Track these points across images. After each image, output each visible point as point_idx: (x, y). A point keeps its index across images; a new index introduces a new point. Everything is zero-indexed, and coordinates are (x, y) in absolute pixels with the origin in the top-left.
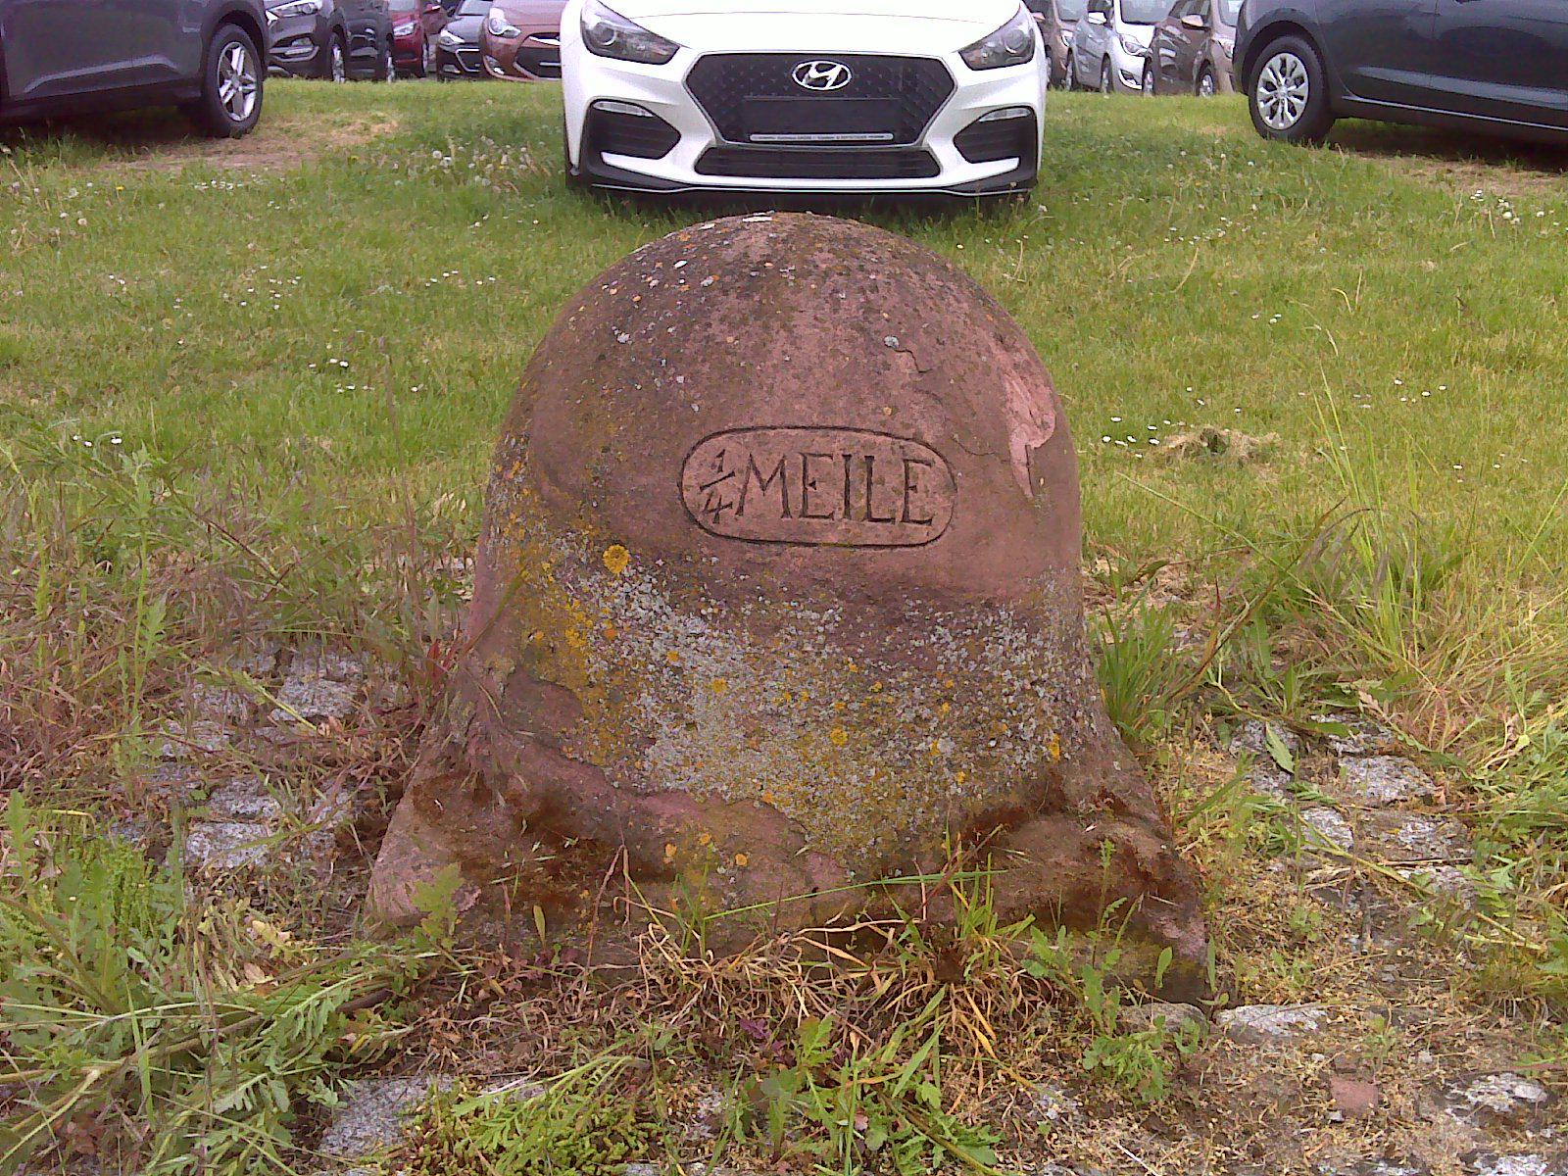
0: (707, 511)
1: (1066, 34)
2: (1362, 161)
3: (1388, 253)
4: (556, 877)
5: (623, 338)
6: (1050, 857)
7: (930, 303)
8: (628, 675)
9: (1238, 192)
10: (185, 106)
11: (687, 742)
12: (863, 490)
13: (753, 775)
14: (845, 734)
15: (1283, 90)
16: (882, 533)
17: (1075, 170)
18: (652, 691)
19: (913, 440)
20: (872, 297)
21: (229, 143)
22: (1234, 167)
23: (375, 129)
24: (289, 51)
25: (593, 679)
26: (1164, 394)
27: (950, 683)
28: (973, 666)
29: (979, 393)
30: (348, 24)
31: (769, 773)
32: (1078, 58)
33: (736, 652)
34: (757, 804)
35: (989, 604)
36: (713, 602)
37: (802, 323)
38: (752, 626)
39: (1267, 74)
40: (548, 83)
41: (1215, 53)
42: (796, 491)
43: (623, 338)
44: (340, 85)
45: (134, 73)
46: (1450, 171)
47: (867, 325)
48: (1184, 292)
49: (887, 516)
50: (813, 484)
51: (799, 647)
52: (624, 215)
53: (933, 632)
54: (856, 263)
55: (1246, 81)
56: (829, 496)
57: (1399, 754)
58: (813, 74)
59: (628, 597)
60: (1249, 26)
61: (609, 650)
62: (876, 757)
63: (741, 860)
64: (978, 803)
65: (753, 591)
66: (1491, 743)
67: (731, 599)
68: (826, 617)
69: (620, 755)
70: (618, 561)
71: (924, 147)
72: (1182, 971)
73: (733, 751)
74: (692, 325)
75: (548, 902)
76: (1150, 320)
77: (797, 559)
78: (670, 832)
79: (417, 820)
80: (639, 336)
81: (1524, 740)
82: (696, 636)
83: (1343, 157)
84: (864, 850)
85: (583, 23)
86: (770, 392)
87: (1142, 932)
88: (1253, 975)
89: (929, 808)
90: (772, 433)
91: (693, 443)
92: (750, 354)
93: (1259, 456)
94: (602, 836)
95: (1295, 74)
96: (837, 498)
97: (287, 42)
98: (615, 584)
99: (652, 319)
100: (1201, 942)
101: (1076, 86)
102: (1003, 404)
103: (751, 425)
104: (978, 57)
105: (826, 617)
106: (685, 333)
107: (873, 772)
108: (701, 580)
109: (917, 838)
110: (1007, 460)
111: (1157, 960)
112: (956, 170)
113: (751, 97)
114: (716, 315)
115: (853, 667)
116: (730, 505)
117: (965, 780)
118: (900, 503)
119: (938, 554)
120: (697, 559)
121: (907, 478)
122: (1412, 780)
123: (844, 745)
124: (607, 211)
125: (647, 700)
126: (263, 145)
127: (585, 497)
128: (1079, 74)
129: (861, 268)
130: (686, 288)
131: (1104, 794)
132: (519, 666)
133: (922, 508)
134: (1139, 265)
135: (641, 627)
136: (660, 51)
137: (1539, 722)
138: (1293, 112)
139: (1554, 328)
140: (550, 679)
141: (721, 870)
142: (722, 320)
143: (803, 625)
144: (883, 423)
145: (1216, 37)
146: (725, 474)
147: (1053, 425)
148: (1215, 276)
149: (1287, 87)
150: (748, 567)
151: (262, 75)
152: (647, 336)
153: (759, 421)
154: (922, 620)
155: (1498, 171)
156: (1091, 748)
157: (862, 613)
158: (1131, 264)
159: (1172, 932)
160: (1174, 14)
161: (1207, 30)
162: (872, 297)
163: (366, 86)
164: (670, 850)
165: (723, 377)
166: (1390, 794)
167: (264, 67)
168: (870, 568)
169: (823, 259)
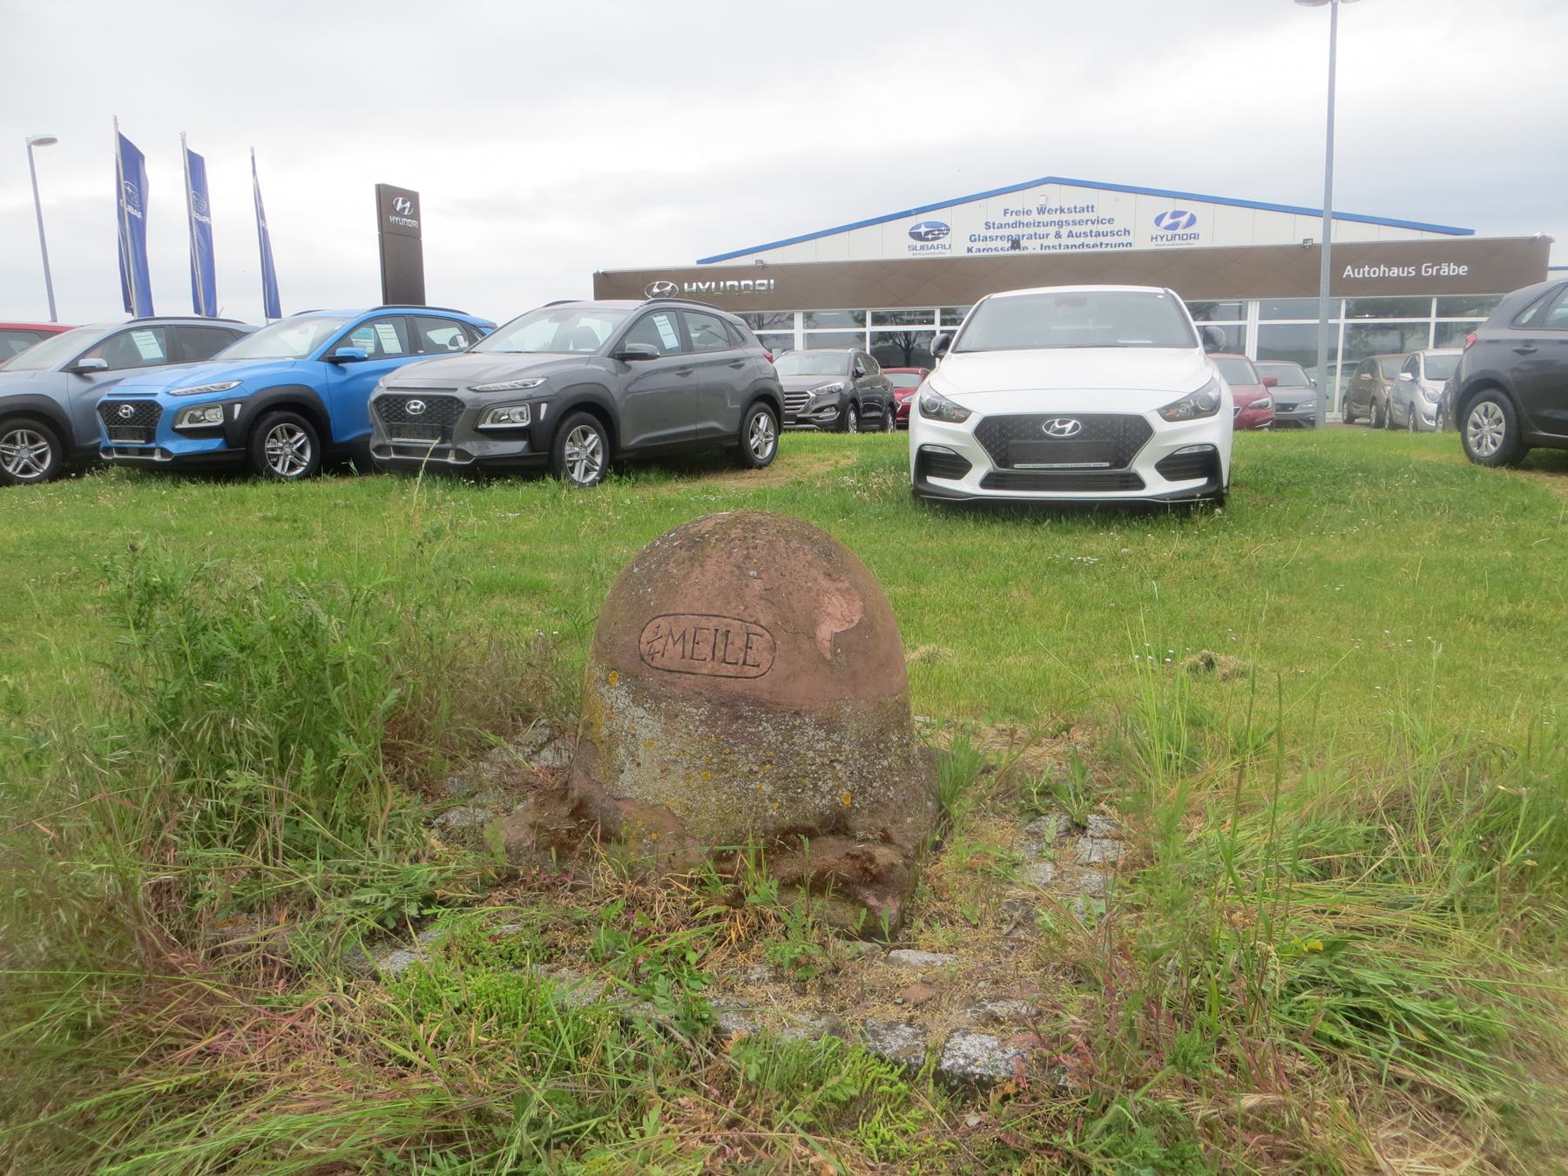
10: (729, 451)
15: (1487, 428)
16: (731, 670)
21: (753, 472)
24: (821, 415)
31: (670, 792)
32: (1394, 405)
35: (797, 713)
37: (710, 565)
39: (1475, 416)
44: (853, 435)
45: (696, 432)
56: (705, 650)
62: (726, 788)
63: (654, 836)
64: (788, 819)
67: (657, 699)
96: (708, 650)
97: (820, 410)
104: (1171, 413)
106: (658, 566)
112: (1157, 486)
119: (763, 684)
125: (622, 750)
138: (1494, 443)
143: (689, 715)
150: (664, 683)
151: (779, 429)
154: (753, 718)
168: (724, 687)
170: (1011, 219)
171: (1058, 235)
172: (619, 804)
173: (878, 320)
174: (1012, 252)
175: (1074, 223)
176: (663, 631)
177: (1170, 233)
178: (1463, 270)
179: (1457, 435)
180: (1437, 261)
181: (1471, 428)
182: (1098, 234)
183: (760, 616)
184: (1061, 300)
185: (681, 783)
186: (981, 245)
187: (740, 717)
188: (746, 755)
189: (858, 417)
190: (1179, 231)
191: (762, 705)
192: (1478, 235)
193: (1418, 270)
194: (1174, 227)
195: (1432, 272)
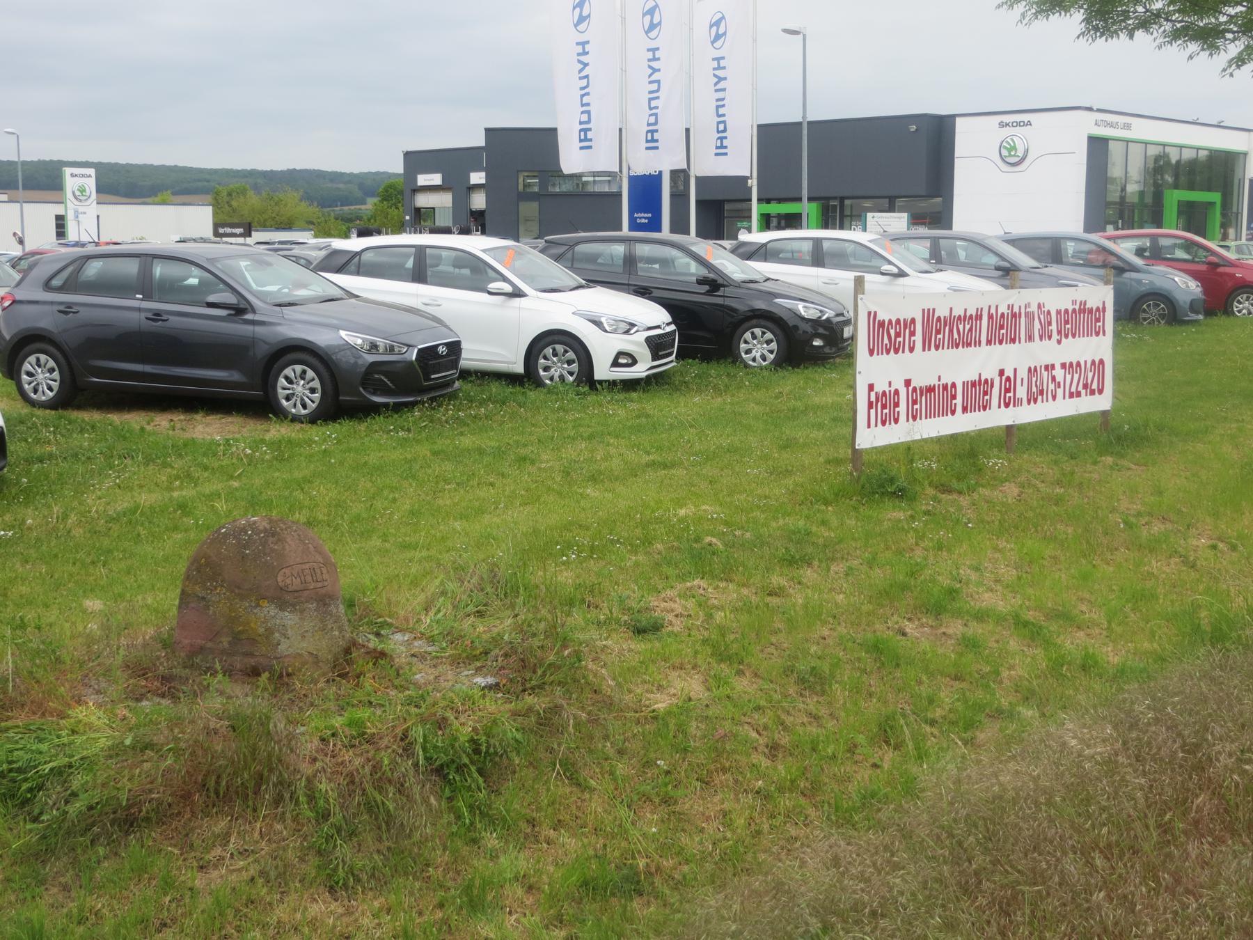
15: (40, 377)
16: (320, 585)
31: (304, 646)
39: (27, 366)
56: (309, 578)
67: (293, 605)
70: (265, 603)
77: (306, 593)
138: (50, 389)
149: (42, 375)
179: (10, 385)
181: (24, 377)
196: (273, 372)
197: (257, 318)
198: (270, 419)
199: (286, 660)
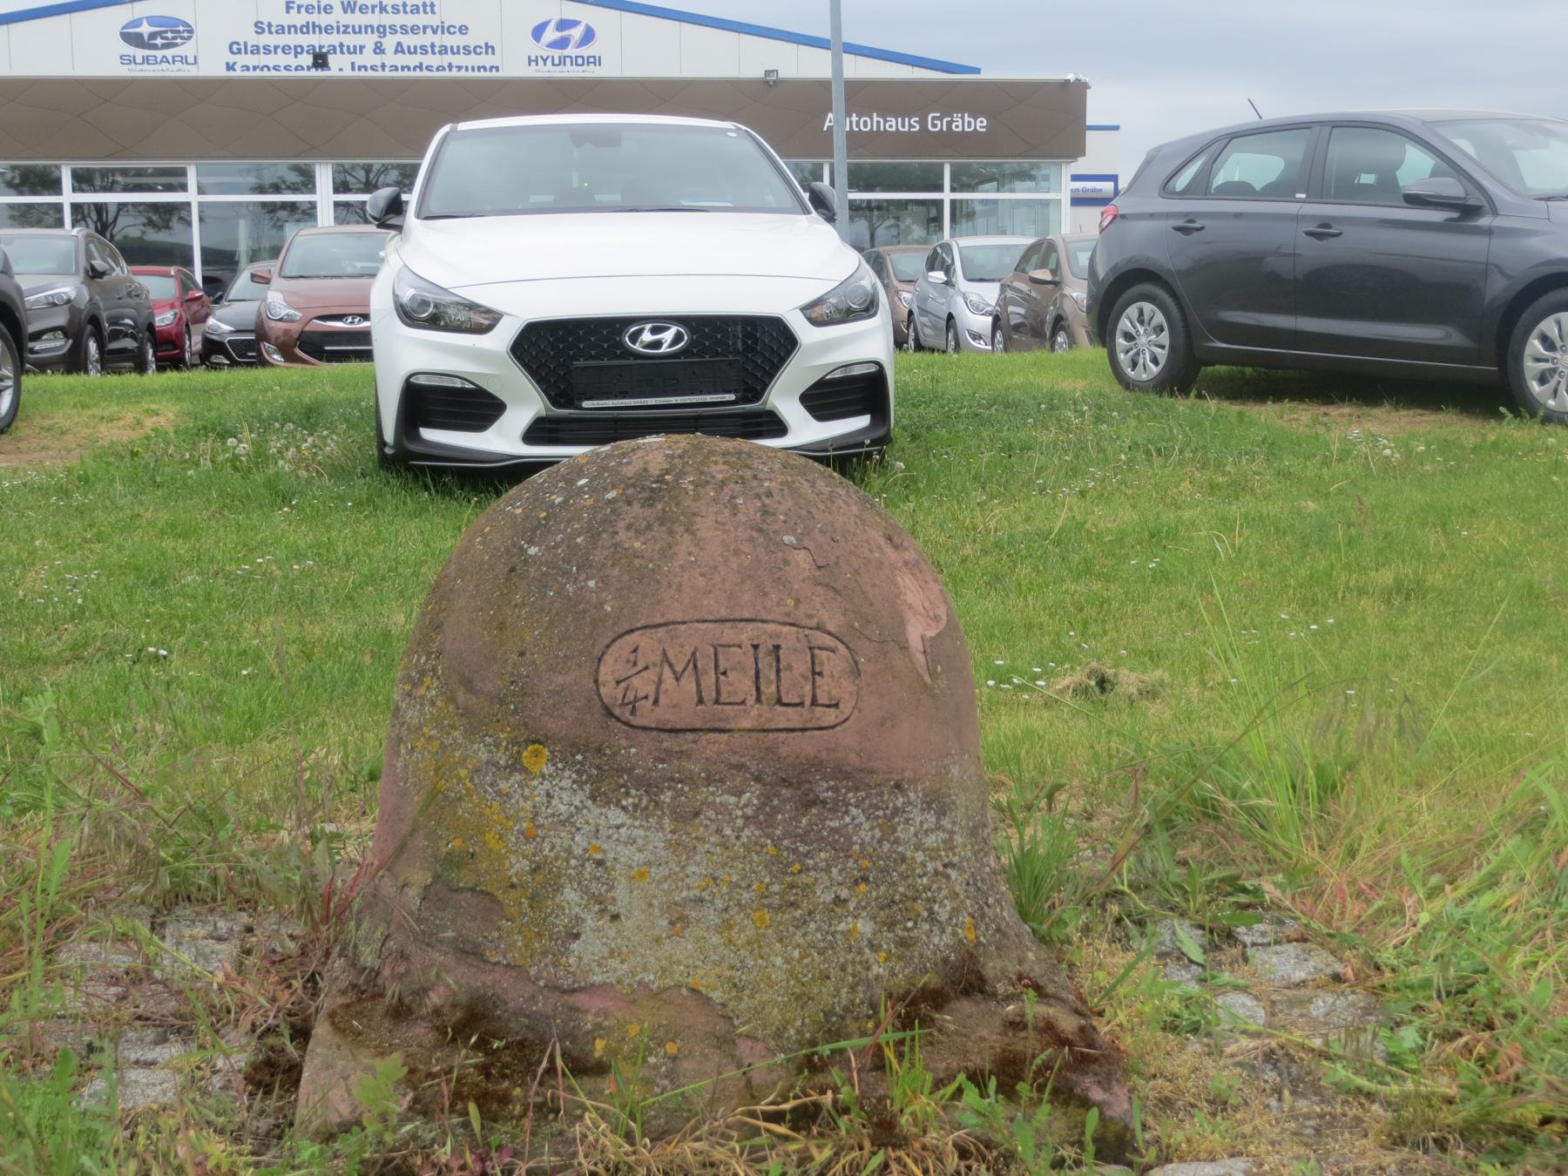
0: (623, 704)
1: (905, 295)
2: (1233, 408)
3: (1268, 497)
4: (488, 1076)
5: (533, 550)
6: (975, 1029)
7: (822, 507)
8: (550, 871)
9: (1104, 444)
11: (612, 933)
12: (773, 676)
13: (679, 963)
14: (767, 917)
15: (1142, 340)
16: (791, 717)
17: (929, 428)
18: (575, 885)
19: (818, 628)
20: (767, 501)
22: (1098, 419)
23: (149, 422)
25: (515, 880)
26: (1047, 641)
27: (865, 863)
28: (886, 846)
29: (874, 585)
30: (104, 315)
31: (694, 957)
32: (920, 319)
33: (658, 841)
34: (684, 991)
36: (633, 792)
37: (704, 527)
38: (673, 812)
39: (1125, 324)
40: (354, 367)
41: (1068, 309)
42: (709, 680)
43: (533, 550)
44: (94, 377)
46: (1325, 414)
47: (765, 526)
48: (1058, 543)
49: (797, 701)
50: (724, 673)
51: (719, 831)
52: (446, 492)
53: (847, 812)
54: (749, 473)
55: (1104, 330)
56: (741, 684)
57: (1305, 940)
58: (647, 337)
59: (548, 795)
60: (1101, 274)
61: (530, 848)
62: (798, 939)
63: (671, 1048)
65: (671, 779)
66: (1394, 925)
67: (651, 787)
68: (744, 800)
69: (544, 953)
71: (768, 407)
72: (1110, 1135)
73: (658, 940)
74: (599, 534)
75: (483, 1099)
76: (1024, 570)
77: (712, 745)
78: (599, 1026)
79: (337, 1040)
80: (548, 548)
81: (1424, 918)
82: (618, 827)
83: (1212, 404)
84: (792, 1031)
85: (395, 296)
86: (679, 588)
87: (1068, 1097)
88: (1179, 1136)
89: (853, 988)
90: (683, 627)
91: (607, 641)
92: (656, 556)
93: (1151, 694)
94: (530, 1036)
95: (1154, 323)
96: (747, 684)
98: (535, 783)
99: (560, 532)
100: (1126, 1106)
101: (919, 347)
102: (897, 596)
103: (662, 621)
105: (744, 800)
106: (594, 537)
107: (796, 954)
108: (620, 771)
109: (843, 1018)
110: (905, 648)
111: (1083, 1124)
113: (582, 363)
114: (622, 524)
115: (771, 848)
116: (646, 697)
117: (886, 960)
118: (808, 687)
119: (846, 737)
120: (612, 752)
121: (813, 663)
122: (1320, 962)
123: (767, 928)
124: (426, 488)
126: (24, 445)
127: (502, 702)
128: (922, 338)
129: (755, 477)
130: (591, 502)
131: (1020, 978)
132: (437, 877)
133: (829, 693)
134: (1008, 518)
135: (563, 823)
136: (480, 321)
137: (1437, 904)
138: (1155, 361)
139: (1443, 556)
140: (470, 885)
141: (652, 1060)
142: (629, 527)
143: (722, 809)
144: (788, 614)
145: (1067, 291)
146: (640, 667)
147: (944, 617)
148: (1088, 526)
149: (1146, 338)
152: (557, 546)
153: (670, 617)
154: (835, 801)
155: (1377, 412)
156: (1004, 935)
157: (777, 795)
158: (998, 517)
159: (1097, 1094)
160: (1020, 268)
161: (1056, 284)
162: (767, 501)
163: (132, 379)
164: (600, 1045)
165: (632, 578)
166: (1299, 975)
167: (22, 360)
169: (719, 470)
170: (299, 19)
171: (379, 49)
172: (580, 999)
173: (83, 180)
174: (314, 73)
175: (404, 30)
176: (649, 654)
177: (557, 53)
178: (981, 124)
179: (1102, 352)
180: (947, 111)
181: (1121, 341)
182: (444, 50)
183: (824, 615)
184: (579, 136)
185: (715, 939)
186: (251, 60)
187: (813, 803)
188: (827, 870)
189: (101, 347)
190: (571, 51)
191: (847, 776)
192: (986, 75)
193: (923, 123)
194: (562, 43)
195: (941, 126)
196: (1520, 326)
197: (1498, 222)
198: (1501, 417)
199: (594, 1004)
